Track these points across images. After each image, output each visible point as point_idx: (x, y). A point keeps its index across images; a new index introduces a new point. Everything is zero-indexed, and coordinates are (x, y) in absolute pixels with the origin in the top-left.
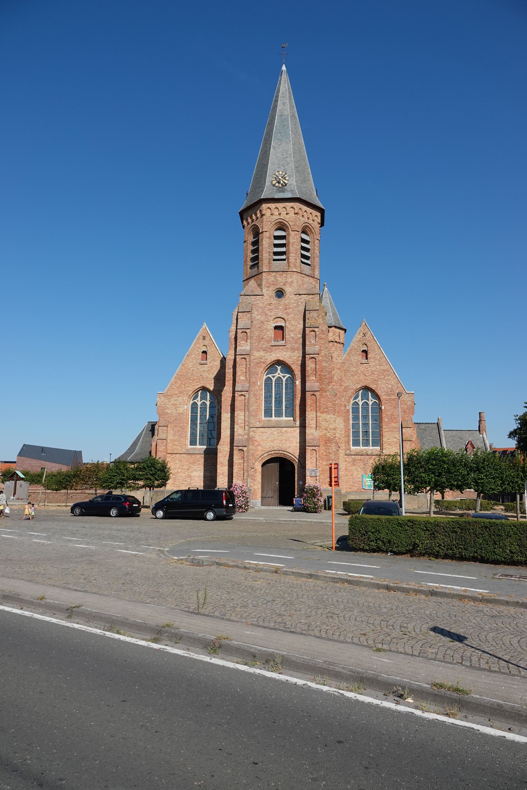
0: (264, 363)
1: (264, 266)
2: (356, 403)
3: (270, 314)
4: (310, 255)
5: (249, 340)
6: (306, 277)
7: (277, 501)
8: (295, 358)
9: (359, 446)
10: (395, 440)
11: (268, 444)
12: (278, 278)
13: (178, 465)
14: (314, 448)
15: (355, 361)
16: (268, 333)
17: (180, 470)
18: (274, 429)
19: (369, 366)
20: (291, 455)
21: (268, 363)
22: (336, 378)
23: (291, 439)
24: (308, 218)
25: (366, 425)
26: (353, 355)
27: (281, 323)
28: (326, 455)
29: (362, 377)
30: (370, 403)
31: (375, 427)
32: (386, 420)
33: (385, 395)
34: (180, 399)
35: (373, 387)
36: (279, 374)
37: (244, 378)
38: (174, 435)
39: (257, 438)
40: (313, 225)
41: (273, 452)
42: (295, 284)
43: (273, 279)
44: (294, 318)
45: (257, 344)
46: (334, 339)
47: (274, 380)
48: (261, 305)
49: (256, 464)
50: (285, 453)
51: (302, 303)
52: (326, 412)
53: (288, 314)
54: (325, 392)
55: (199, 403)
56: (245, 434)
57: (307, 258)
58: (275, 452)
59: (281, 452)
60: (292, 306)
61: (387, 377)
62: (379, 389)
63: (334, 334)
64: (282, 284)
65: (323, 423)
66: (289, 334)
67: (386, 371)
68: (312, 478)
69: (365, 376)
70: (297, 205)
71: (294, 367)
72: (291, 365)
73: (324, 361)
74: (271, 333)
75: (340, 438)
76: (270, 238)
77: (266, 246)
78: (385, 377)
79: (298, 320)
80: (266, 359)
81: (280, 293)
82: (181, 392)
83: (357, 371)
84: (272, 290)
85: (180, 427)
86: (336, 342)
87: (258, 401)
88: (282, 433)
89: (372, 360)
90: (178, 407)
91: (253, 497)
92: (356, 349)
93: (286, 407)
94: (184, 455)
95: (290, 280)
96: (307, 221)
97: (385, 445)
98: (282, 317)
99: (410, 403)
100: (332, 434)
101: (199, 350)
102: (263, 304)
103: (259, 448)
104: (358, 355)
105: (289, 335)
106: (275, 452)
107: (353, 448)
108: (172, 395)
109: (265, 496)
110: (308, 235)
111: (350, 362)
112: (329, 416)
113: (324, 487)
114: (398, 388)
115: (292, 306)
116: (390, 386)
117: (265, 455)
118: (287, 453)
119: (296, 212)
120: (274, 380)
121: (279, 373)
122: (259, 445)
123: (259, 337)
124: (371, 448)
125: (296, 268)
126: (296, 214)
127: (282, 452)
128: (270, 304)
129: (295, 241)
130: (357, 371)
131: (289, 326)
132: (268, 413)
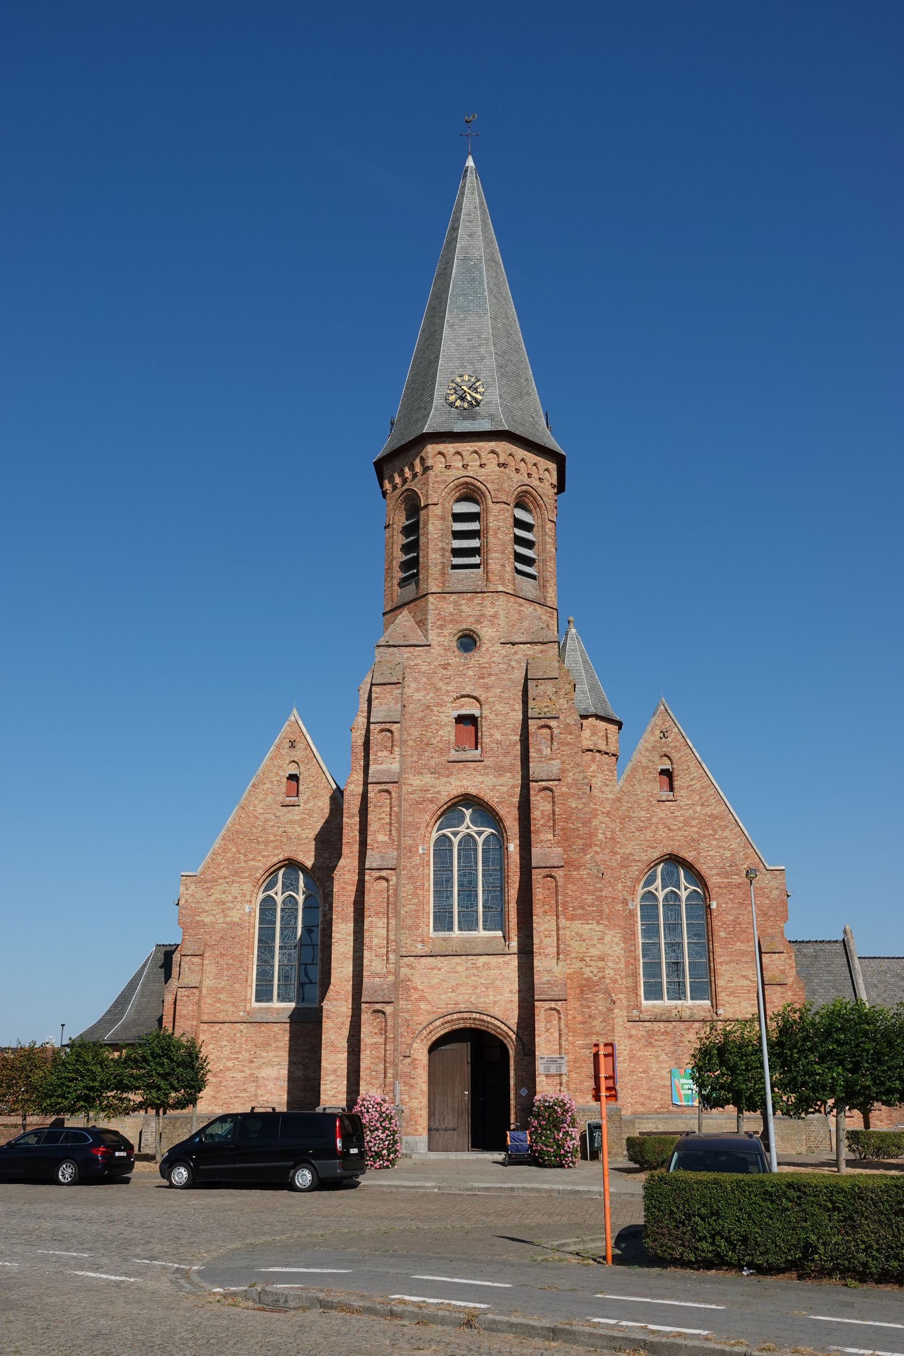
0: (432, 801)
1: (430, 580)
2: (650, 895)
5: (396, 749)
7: (466, 1139)
8: (504, 789)
10: (747, 982)
11: (443, 997)
12: (464, 608)
13: (226, 1052)
14: (553, 1005)
16: (441, 733)
17: (230, 1064)
18: (457, 960)
19: (678, 805)
20: (499, 1024)
22: (600, 836)
23: (498, 983)
24: (529, 475)
25: (675, 947)
26: (639, 781)
27: (472, 709)
28: (583, 1023)
29: (662, 833)
30: (684, 894)
31: (697, 953)
32: (723, 934)
33: (718, 874)
34: (235, 890)
35: (689, 856)
36: (468, 828)
39: (417, 982)
40: (540, 490)
41: (455, 1016)
42: (502, 621)
44: (500, 697)
45: (415, 758)
47: (456, 841)
48: (424, 668)
49: (415, 1045)
50: (485, 1018)
51: (518, 662)
52: (581, 917)
53: (487, 688)
54: (578, 868)
55: (279, 899)
56: (389, 972)
58: (460, 1015)
59: (474, 1015)
60: (495, 670)
61: (720, 832)
63: (594, 733)
66: (490, 735)
67: (716, 818)
69: (670, 829)
71: (502, 811)
72: (494, 805)
74: (449, 732)
76: (443, 518)
77: (436, 536)
78: (715, 831)
79: (511, 702)
80: (438, 793)
81: (468, 641)
82: (236, 873)
83: (649, 819)
86: (599, 751)
87: (420, 892)
89: (683, 792)
90: (230, 909)
93: (484, 907)
94: (242, 1027)
95: (490, 611)
96: (526, 480)
97: (722, 996)
98: (474, 694)
101: (281, 773)
102: (429, 665)
103: (423, 1006)
104: (650, 781)
106: (460, 1015)
107: (645, 1003)
108: (214, 880)
109: (436, 1126)
110: (528, 510)
111: (634, 798)
112: (588, 927)
114: (746, 858)
115: (495, 670)
119: (502, 461)
120: (456, 841)
122: (423, 998)
123: (421, 741)
124: (690, 1002)
125: (503, 584)
127: (478, 1016)
128: (445, 667)
130: (649, 819)
131: (491, 716)
132: (443, 921)
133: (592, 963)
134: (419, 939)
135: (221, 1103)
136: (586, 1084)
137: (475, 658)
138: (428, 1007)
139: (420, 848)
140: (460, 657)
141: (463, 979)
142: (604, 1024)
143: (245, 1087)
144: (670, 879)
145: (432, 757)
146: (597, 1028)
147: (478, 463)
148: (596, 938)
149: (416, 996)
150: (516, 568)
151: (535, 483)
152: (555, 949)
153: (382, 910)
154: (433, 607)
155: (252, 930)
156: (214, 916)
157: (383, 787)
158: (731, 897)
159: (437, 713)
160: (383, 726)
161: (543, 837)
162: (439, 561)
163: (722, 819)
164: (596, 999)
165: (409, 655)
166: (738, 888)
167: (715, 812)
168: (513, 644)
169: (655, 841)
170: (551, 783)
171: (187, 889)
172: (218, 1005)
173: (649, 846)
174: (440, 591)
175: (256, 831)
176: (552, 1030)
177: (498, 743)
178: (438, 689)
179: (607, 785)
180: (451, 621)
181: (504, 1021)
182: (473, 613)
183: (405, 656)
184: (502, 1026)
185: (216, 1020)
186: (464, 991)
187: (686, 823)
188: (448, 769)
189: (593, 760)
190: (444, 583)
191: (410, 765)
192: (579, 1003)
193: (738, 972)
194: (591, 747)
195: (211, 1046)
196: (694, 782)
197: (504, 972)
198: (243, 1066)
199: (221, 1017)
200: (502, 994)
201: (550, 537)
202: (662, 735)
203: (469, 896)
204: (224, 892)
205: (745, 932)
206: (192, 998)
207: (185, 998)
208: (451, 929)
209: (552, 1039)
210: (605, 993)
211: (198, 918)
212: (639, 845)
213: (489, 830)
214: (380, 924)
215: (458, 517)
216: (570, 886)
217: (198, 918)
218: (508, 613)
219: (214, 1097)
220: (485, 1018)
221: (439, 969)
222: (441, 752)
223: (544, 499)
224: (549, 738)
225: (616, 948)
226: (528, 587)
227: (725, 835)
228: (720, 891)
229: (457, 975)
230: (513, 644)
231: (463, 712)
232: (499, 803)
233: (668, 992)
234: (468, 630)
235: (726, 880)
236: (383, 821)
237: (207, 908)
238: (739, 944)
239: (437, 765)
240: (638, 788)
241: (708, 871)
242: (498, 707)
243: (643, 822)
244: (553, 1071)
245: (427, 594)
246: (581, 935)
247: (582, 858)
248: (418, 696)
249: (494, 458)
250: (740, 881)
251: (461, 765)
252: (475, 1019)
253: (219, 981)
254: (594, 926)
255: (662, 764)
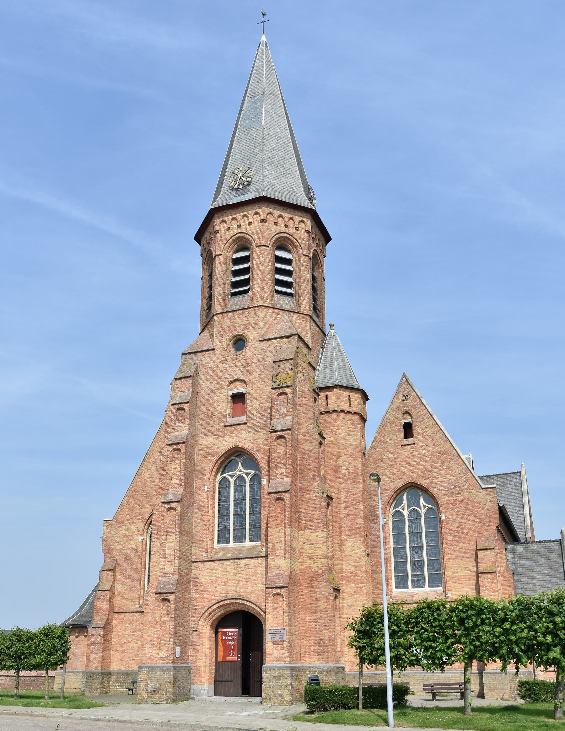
0: (214, 455)
2: (398, 514)
3: (223, 376)
4: (292, 281)
6: (283, 313)
7: (240, 689)
8: (260, 441)
9: (407, 587)
10: (468, 573)
12: (237, 320)
13: (128, 632)
14: (278, 591)
15: (393, 442)
16: (220, 407)
17: (130, 639)
18: (228, 562)
19: (416, 447)
20: (254, 607)
21: (220, 454)
22: (343, 471)
23: (254, 578)
24: (286, 226)
25: (417, 549)
26: (388, 433)
27: (239, 388)
28: (311, 604)
29: (405, 468)
30: (422, 511)
31: (434, 553)
32: (450, 538)
33: (446, 494)
34: (133, 527)
35: (424, 482)
36: (240, 471)
37: (177, 481)
38: (124, 583)
39: (203, 579)
40: (296, 236)
41: (226, 602)
42: (261, 326)
43: (228, 322)
44: (259, 378)
45: (204, 426)
46: (338, 407)
47: (232, 481)
48: (211, 365)
50: (245, 602)
51: (271, 352)
52: (310, 528)
53: (250, 372)
54: (309, 493)
56: (174, 572)
57: (289, 285)
58: (229, 601)
59: (238, 601)
60: (256, 360)
61: (447, 463)
62: (434, 485)
63: (338, 399)
64: (241, 328)
65: (305, 547)
66: (251, 404)
67: (444, 453)
68: (276, 646)
69: (410, 465)
70: (263, 211)
71: (259, 456)
72: (254, 453)
73: (306, 441)
74: (226, 406)
75: (356, 574)
76: (225, 263)
77: (220, 276)
78: (443, 463)
79: (266, 380)
80: (218, 448)
81: (239, 342)
82: (134, 517)
83: (396, 459)
84: (227, 340)
85: (132, 570)
86: (343, 411)
87: (205, 517)
88: (240, 568)
89: (420, 438)
90: (130, 540)
91: (195, 681)
92: (394, 422)
93: (250, 525)
94: (136, 615)
95: (253, 320)
96: (283, 229)
97: (450, 583)
98: (242, 378)
99: (489, 504)
100: (320, 566)
103: (206, 595)
104: (396, 432)
105: (252, 405)
106: (229, 601)
107: (395, 591)
108: (122, 522)
109: (220, 679)
110: (289, 251)
111: (385, 445)
112: (315, 534)
113: (309, 660)
114: (467, 481)
115: (256, 360)
116: (453, 479)
117: (215, 607)
118: (248, 603)
119: (262, 218)
120: (232, 481)
121: (240, 470)
122: (206, 590)
123: (208, 414)
124: (428, 589)
125: (262, 301)
126: (263, 221)
127: (240, 601)
129: (261, 260)
130: (396, 459)
131: (252, 392)
132: (223, 537)
133: (318, 560)
134: (204, 550)
135: (125, 663)
136: (313, 648)
137: (246, 352)
138: (209, 596)
139: (206, 487)
140: (233, 354)
141: (232, 575)
142: (326, 604)
143: (139, 653)
144: (413, 501)
145: (214, 424)
146: (321, 608)
147: (247, 223)
148: (321, 542)
149: (202, 589)
150: (275, 289)
151: (291, 230)
152: (283, 551)
153: (172, 530)
154: (217, 323)
155: (144, 553)
156: (122, 545)
157: (176, 447)
158: (456, 510)
159: (218, 394)
160: (179, 406)
161: (278, 471)
162: (222, 292)
163: (448, 454)
164: (320, 586)
165: (201, 357)
166: (461, 503)
167: (443, 449)
168: (268, 340)
169: (400, 474)
170: (284, 432)
171: (107, 529)
172: (123, 601)
173: (396, 478)
174: (222, 311)
175: (145, 489)
176: (278, 609)
177: (257, 409)
178: (219, 378)
179: (350, 435)
180: (228, 330)
181: (257, 604)
182: (243, 323)
183: (199, 358)
184: (257, 608)
185: (122, 611)
186: (232, 584)
187: (422, 459)
188: (224, 432)
189: (338, 417)
190: (225, 306)
191: (200, 431)
192: (309, 590)
193: (461, 565)
194: (336, 409)
195: (120, 627)
196: (428, 429)
197: (258, 569)
198: (137, 640)
199: (125, 609)
200: (256, 585)
201: (304, 266)
202: (404, 398)
203: (241, 518)
204: (128, 529)
205: (466, 535)
206: (106, 597)
207: (102, 597)
208: (228, 542)
209: (278, 616)
210: (326, 582)
211: (113, 547)
212: (389, 478)
213: (253, 472)
214: (171, 540)
215: (236, 261)
216: (303, 506)
217: (113, 547)
218: (265, 320)
219: (121, 660)
220: (245, 602)
221: (216, 570)
222: (220, 420)
223: (300, 241)
224: (286, 401)
225: (357, 551)
226: (285, 302)
227: (451, 465)
228: (447, 506)
229: (228, 573)
230: (268, 340)
231: (235, 391)
232: (257, 451)
233: (412, 582)
234: (238, 335)
235: (452, 498)
236: (176, 470)
237: (118, 540)
238: (462, 544)
239: (218, 429)
240: (388, 438)
241: (438, 493)
242: (257, 385)
243: (391, 461)
244: (277, 639)
245: (214, 315)
246: (311, 541)
247: (312, 485)
248: (206, 384)
249: (258, 217)
250: (462, 498)
251: (232, 428)
252: (239, 603)
253: (124, 586)
254: (320, 533)
255: (405, 419)
